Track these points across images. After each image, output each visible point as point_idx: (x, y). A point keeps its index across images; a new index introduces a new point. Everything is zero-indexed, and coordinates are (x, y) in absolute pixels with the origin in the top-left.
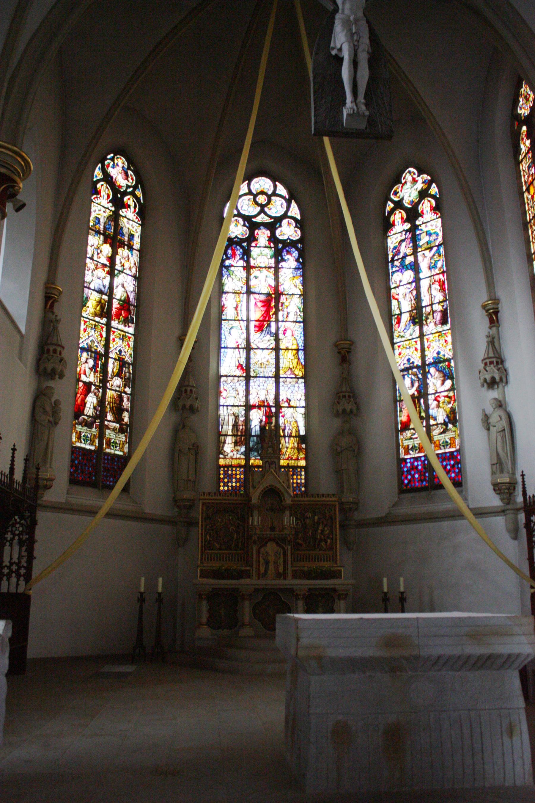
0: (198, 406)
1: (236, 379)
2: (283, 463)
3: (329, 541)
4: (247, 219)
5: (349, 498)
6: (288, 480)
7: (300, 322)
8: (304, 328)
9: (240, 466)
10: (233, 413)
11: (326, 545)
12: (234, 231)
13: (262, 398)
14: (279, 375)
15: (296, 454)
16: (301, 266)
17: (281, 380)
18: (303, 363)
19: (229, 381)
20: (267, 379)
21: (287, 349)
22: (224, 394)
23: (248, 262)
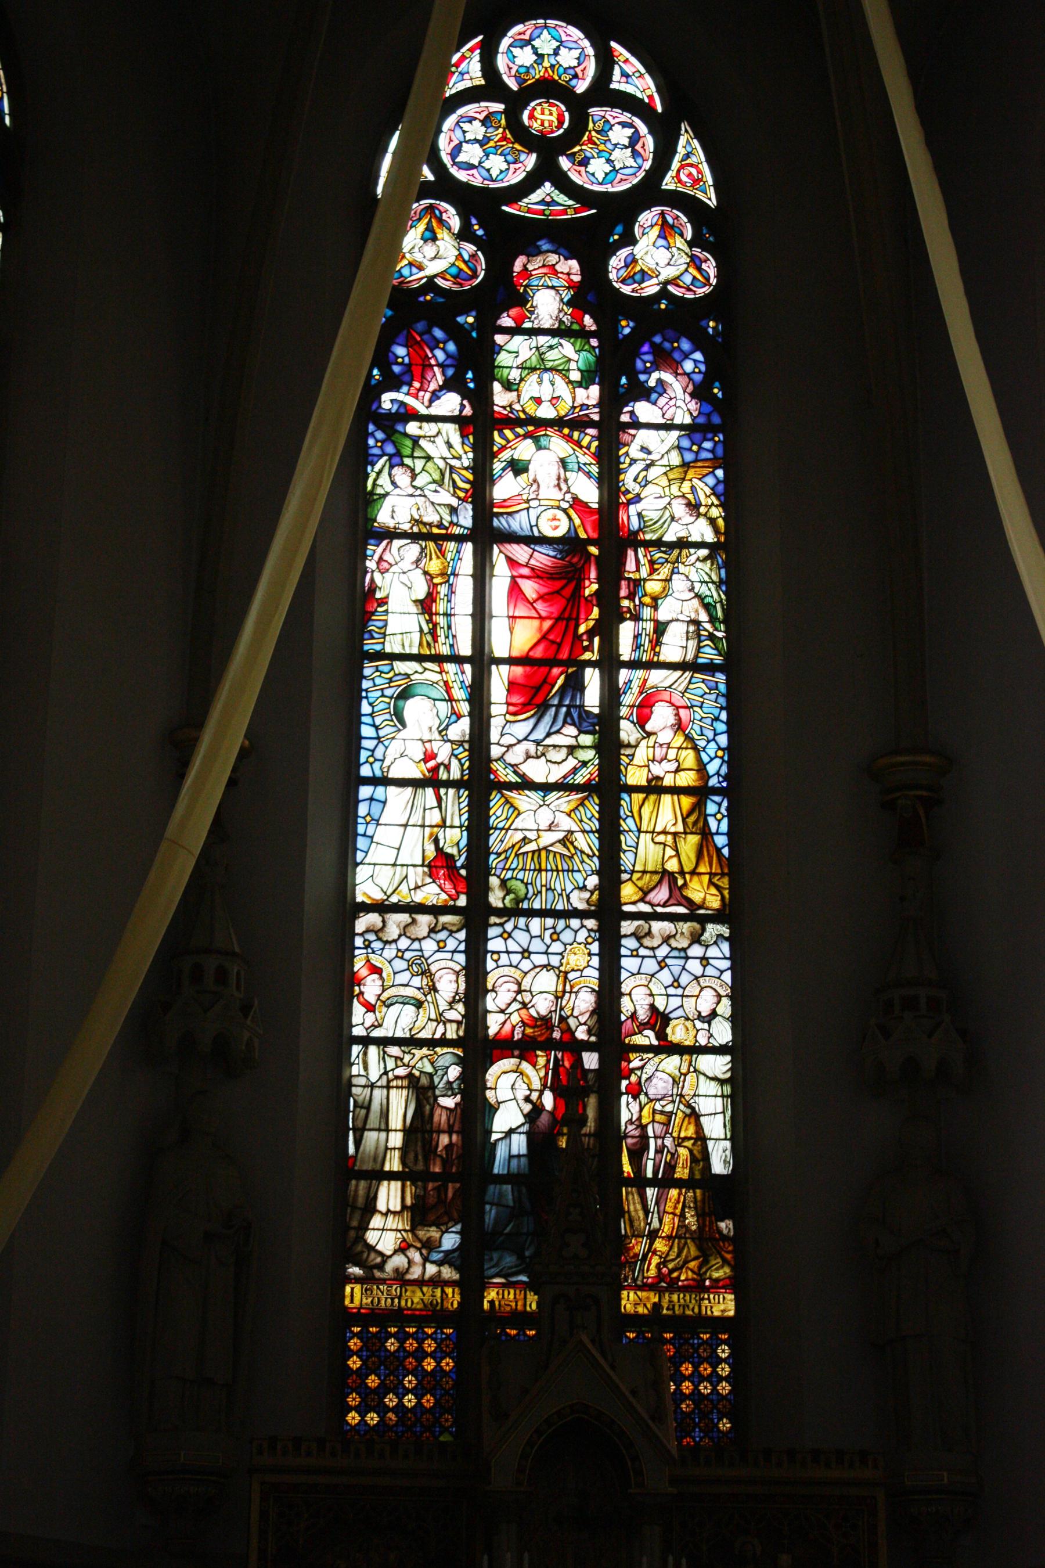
1: (425, 920)
2: (630, 1301)
4: (481, 206)
6: (658, 1386)
7: (710, 668)
8: (728, 696)
9: (434, 1315)
12: (418, 257)
16: (716, 420)
17: (627, 927)
19: (392, 932)
20: (561, 924)
21: (654, 788)
23: (480, 398)
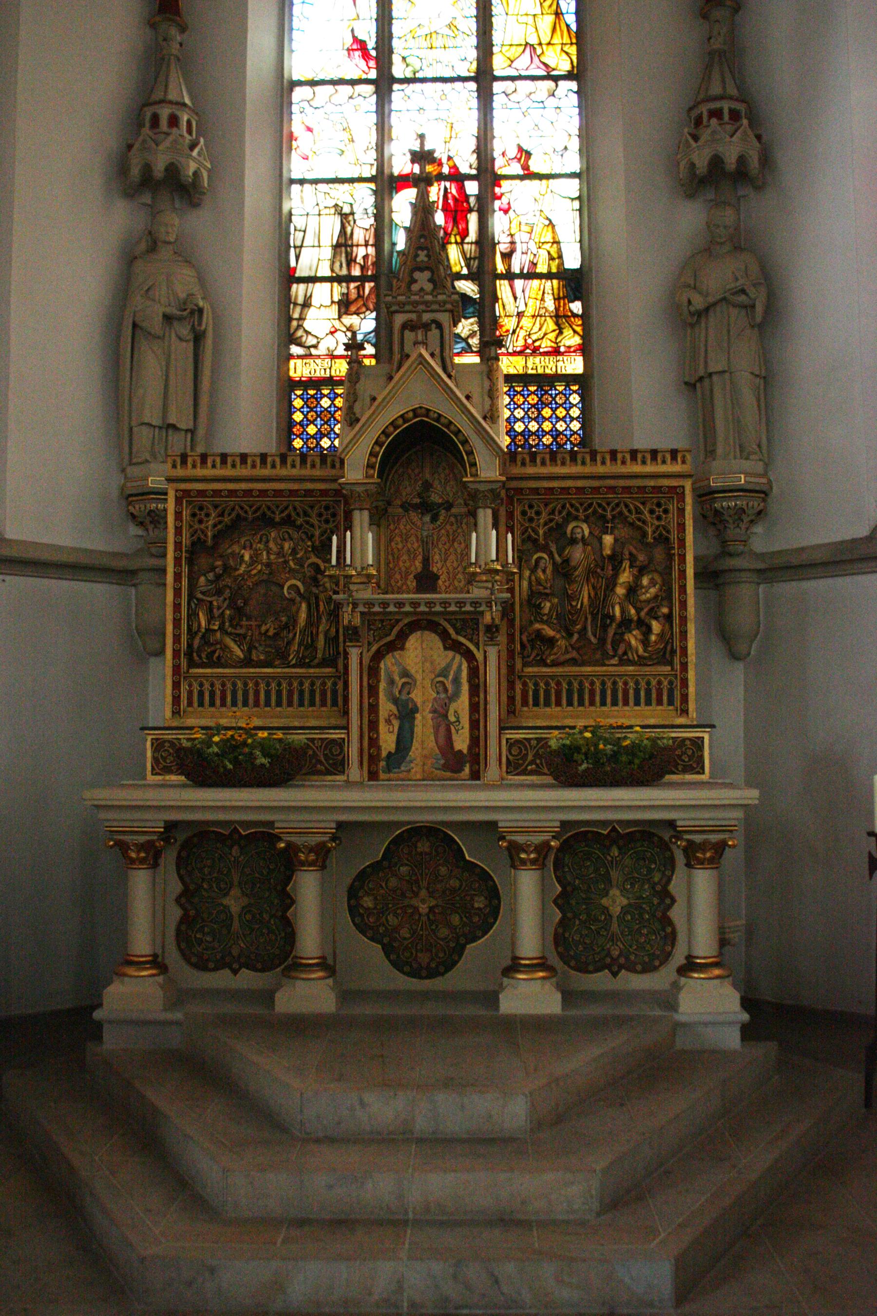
0: (195, 173)
1: (346, 89)
3: (656, 626)
5: (733, 472)
10: (336, 205)
11: (645, 642)
14: (492, 69)
15: (552, 336)
17: (497, 87)
18: (574, 27)
22: (303, 142)
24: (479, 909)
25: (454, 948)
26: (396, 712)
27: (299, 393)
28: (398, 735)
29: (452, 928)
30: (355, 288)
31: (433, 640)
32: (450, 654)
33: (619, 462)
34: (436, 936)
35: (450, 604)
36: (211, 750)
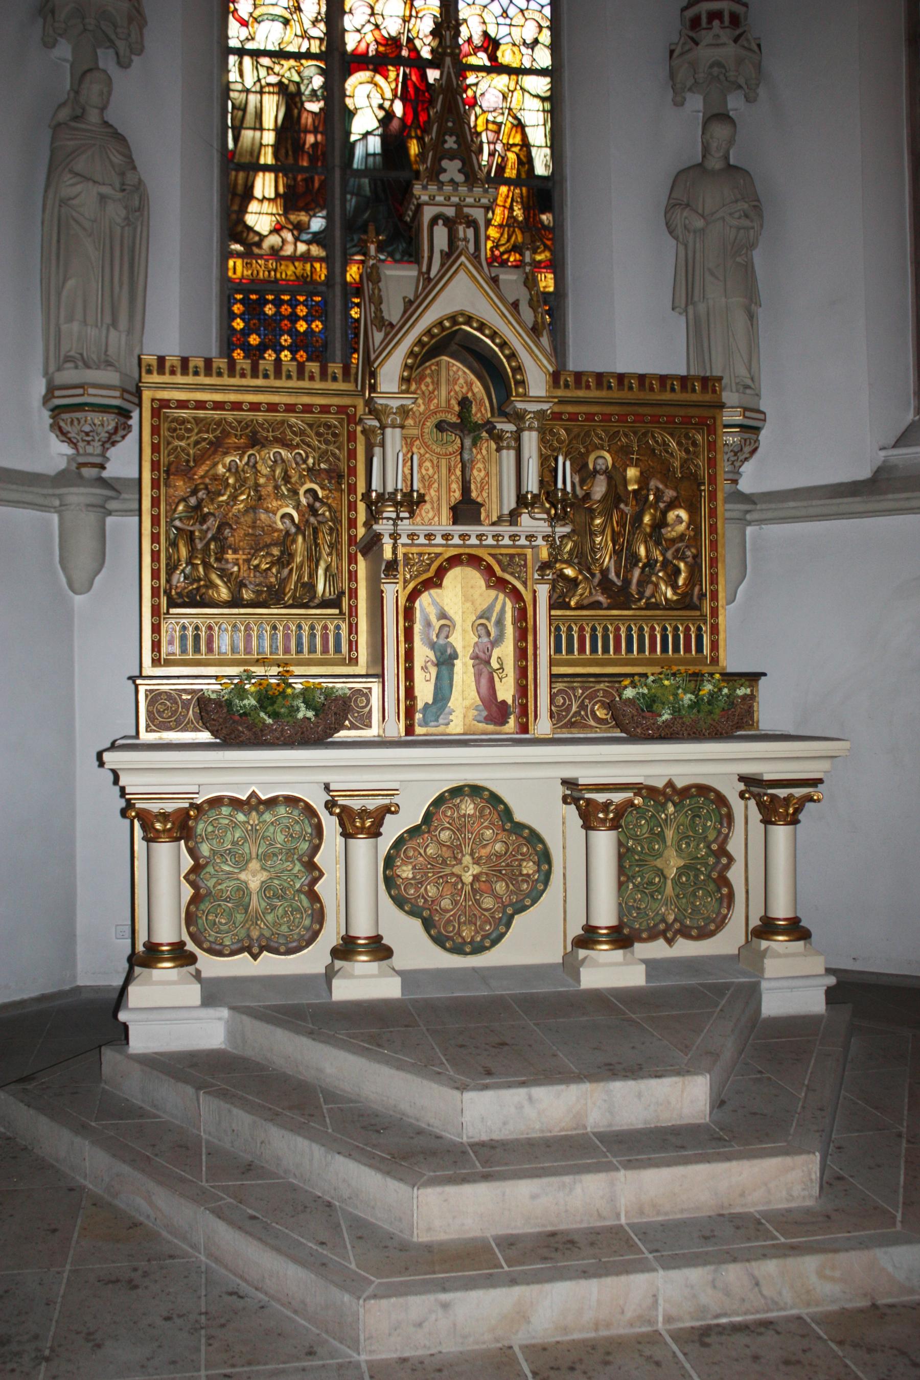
13: (392, 27)
24: (528, 875)
25: (500, 919)
26: (434, 659)
27: (239, 297)
28: (436, 684)
29: (497, 897)
30: (302, 180)
31: (476, 578)
32: (493, 593)
33: (626, 388)
34: (480, 907)
35: (470, 536)
36: (246, 702)
